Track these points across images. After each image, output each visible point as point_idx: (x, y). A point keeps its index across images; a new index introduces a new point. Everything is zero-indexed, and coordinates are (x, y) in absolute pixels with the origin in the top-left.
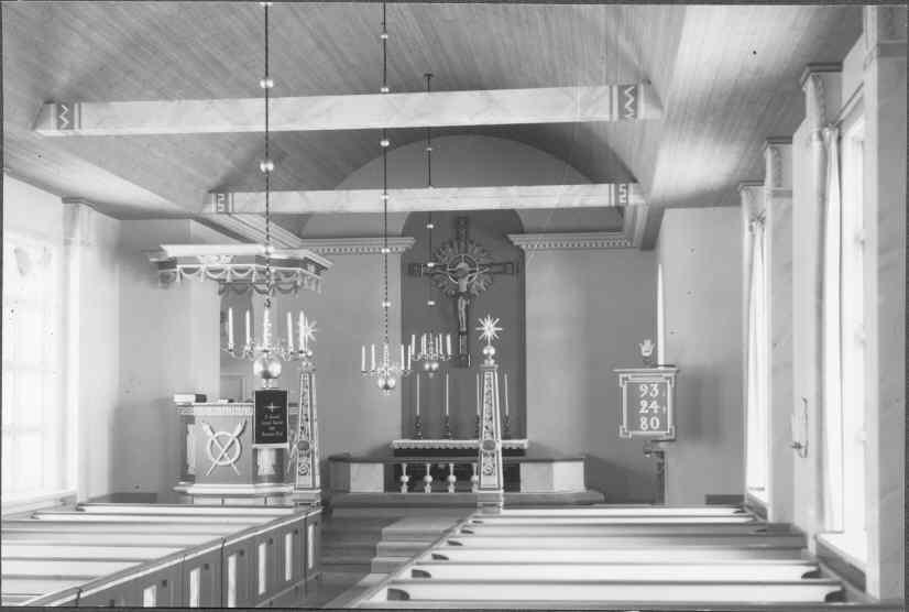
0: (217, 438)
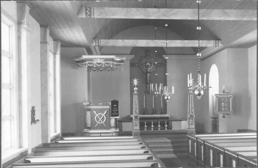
0: (99, 115)
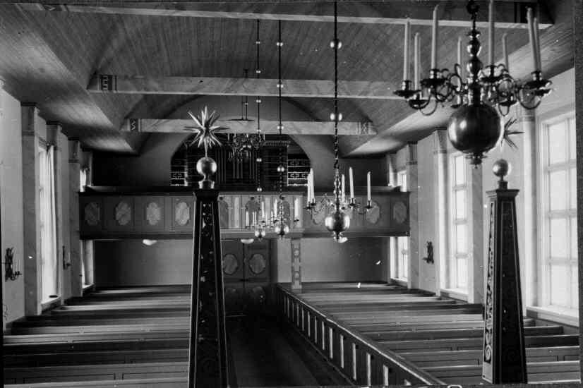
0: (524, 21)
